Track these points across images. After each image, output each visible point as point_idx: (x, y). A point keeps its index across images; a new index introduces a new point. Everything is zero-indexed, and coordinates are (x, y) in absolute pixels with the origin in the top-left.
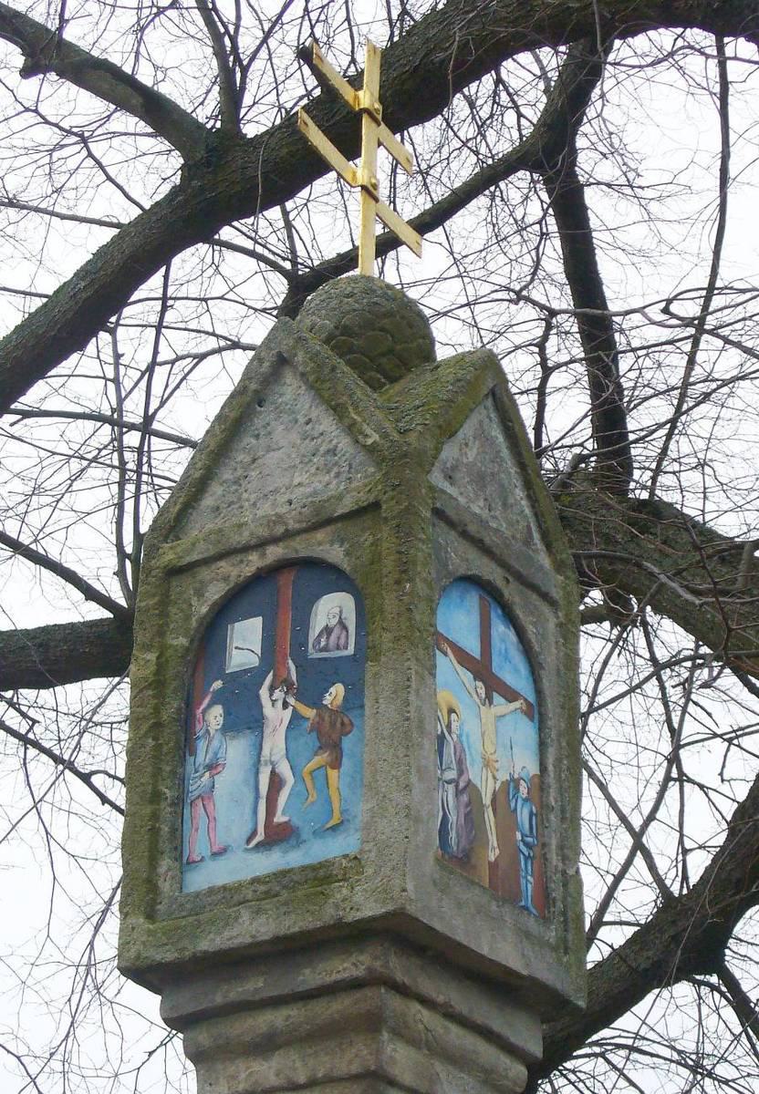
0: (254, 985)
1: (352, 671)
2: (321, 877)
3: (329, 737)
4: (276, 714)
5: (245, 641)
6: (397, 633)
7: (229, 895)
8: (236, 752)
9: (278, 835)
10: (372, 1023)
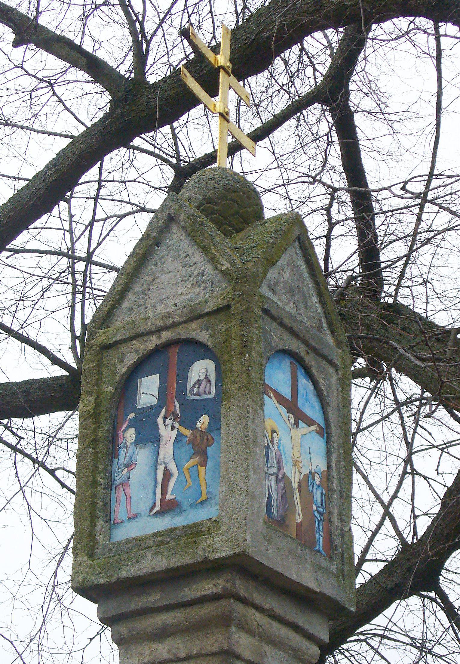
0: (154, 598)
1: (213, 407)
2: (194, 532)
3: (200, 446)
4: (168, 433)
5: (149, 389)
6: (240, 384)
7: (139, 544)
8: (143, 456)
9: (168, 507)
10: (225, 621)
